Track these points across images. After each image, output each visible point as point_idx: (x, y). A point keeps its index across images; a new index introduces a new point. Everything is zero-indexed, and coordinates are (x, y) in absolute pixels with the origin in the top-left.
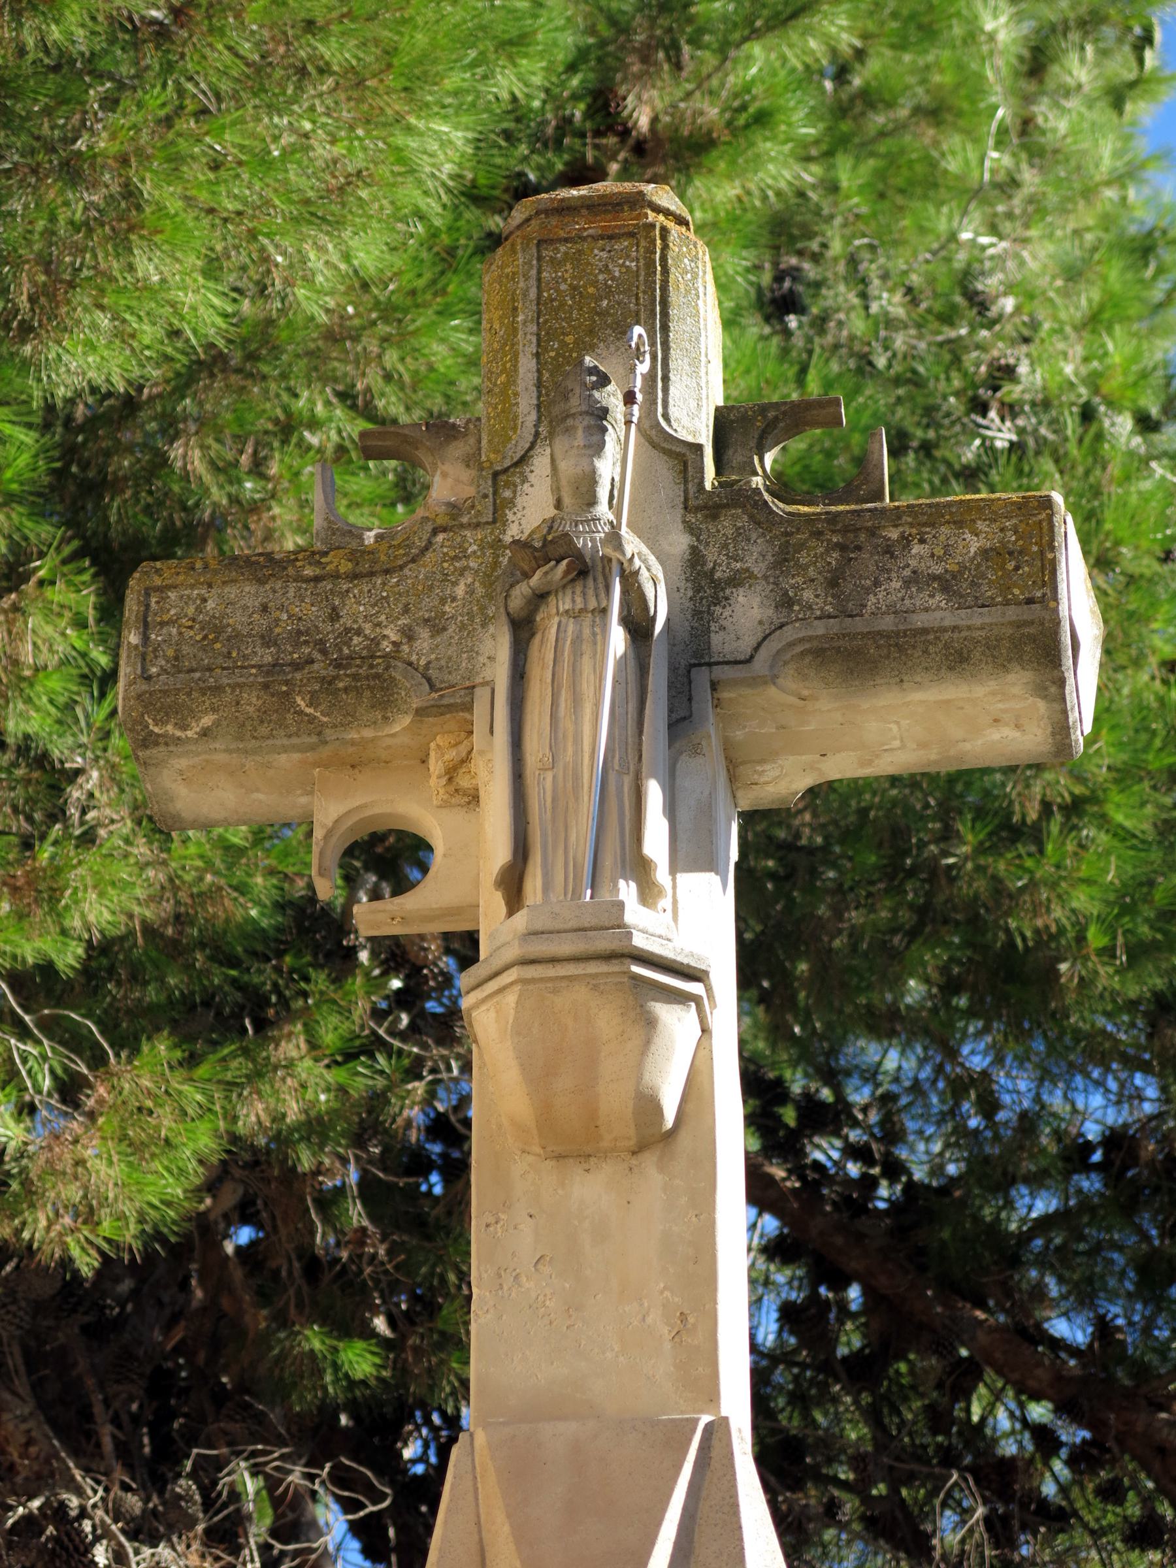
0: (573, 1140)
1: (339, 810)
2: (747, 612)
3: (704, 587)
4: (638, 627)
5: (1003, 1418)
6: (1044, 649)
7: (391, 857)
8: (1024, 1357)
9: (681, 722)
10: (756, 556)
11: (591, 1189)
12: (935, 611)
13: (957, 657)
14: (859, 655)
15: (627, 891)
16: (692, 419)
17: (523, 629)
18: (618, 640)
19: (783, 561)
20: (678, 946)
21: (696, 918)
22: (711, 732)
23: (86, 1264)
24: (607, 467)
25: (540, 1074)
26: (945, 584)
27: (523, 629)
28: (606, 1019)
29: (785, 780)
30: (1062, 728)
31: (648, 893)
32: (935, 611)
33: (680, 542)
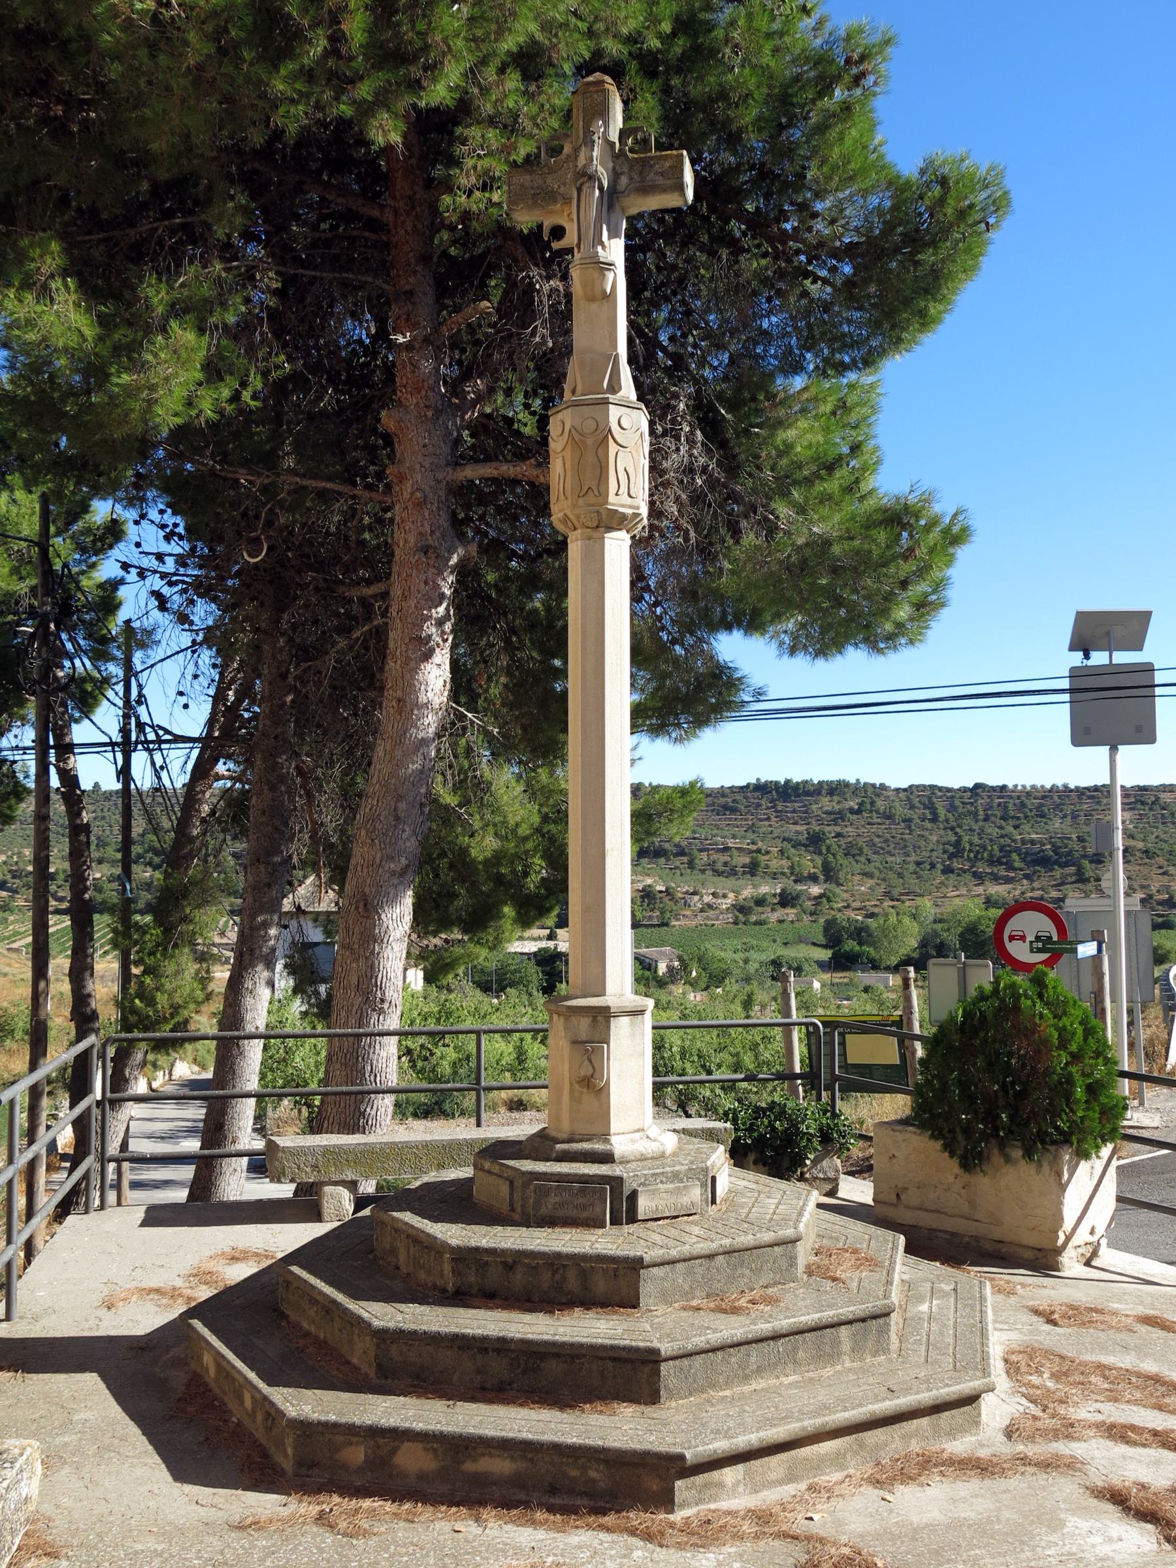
0: (591, 299)
1: (548, 224)
2: (624, 181)
3: (615, 176)
4: (601, 189)
5: (736, 228)
6: (681, 188)
7: (558, 232)
8: (741, 215)
9: (610, 207)
10: (625, 168)
11: (594, 307)
12: (660, 180)
13: (664, 190)
14: (646, 190)
15: (599, 248)
16: (614, 136)
17: (579, 190)
18: (597, 192)
19: (631, 169)
20: (610, 259)
21: (615, 251)
22: (617, 208)
23: (525, 231)
24: (595, 154)
25: (584, 287)
26: (662, 174)
27: (579, 190)
28: (596, 275)
29: (634, 211)
30: (686, 201)
31: (604, 247)
32: (660, 180)
33: (611, 165)
